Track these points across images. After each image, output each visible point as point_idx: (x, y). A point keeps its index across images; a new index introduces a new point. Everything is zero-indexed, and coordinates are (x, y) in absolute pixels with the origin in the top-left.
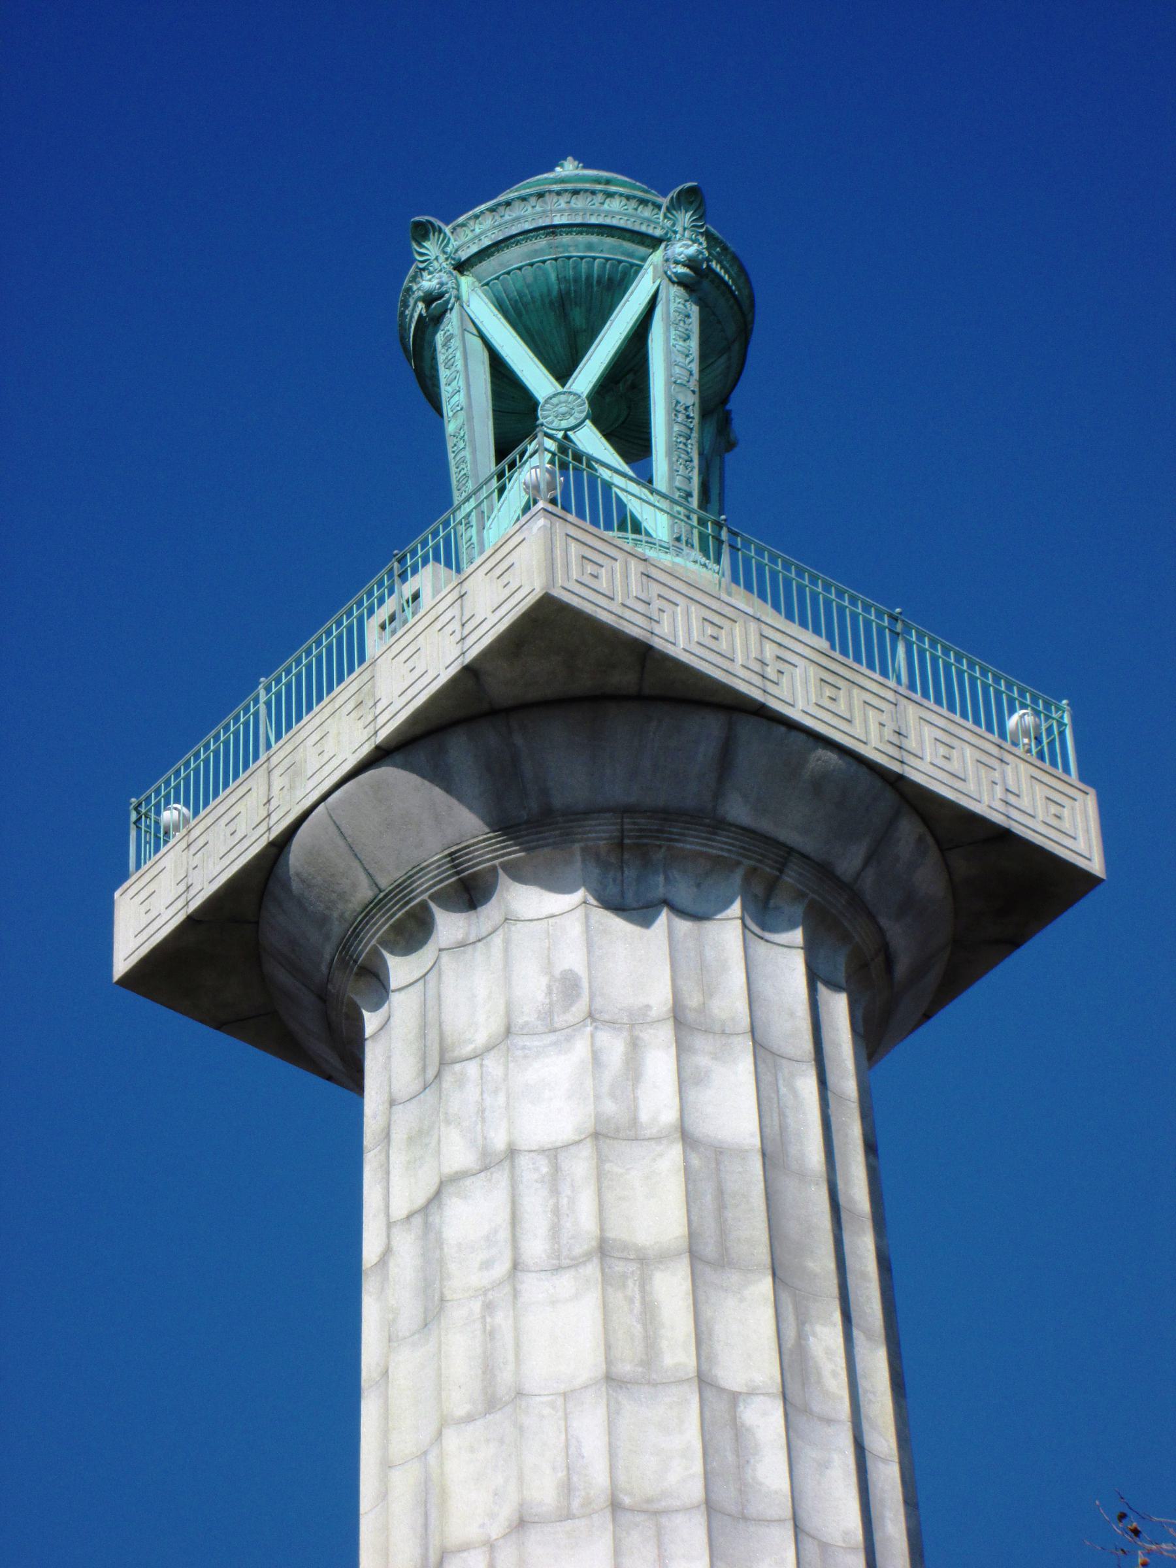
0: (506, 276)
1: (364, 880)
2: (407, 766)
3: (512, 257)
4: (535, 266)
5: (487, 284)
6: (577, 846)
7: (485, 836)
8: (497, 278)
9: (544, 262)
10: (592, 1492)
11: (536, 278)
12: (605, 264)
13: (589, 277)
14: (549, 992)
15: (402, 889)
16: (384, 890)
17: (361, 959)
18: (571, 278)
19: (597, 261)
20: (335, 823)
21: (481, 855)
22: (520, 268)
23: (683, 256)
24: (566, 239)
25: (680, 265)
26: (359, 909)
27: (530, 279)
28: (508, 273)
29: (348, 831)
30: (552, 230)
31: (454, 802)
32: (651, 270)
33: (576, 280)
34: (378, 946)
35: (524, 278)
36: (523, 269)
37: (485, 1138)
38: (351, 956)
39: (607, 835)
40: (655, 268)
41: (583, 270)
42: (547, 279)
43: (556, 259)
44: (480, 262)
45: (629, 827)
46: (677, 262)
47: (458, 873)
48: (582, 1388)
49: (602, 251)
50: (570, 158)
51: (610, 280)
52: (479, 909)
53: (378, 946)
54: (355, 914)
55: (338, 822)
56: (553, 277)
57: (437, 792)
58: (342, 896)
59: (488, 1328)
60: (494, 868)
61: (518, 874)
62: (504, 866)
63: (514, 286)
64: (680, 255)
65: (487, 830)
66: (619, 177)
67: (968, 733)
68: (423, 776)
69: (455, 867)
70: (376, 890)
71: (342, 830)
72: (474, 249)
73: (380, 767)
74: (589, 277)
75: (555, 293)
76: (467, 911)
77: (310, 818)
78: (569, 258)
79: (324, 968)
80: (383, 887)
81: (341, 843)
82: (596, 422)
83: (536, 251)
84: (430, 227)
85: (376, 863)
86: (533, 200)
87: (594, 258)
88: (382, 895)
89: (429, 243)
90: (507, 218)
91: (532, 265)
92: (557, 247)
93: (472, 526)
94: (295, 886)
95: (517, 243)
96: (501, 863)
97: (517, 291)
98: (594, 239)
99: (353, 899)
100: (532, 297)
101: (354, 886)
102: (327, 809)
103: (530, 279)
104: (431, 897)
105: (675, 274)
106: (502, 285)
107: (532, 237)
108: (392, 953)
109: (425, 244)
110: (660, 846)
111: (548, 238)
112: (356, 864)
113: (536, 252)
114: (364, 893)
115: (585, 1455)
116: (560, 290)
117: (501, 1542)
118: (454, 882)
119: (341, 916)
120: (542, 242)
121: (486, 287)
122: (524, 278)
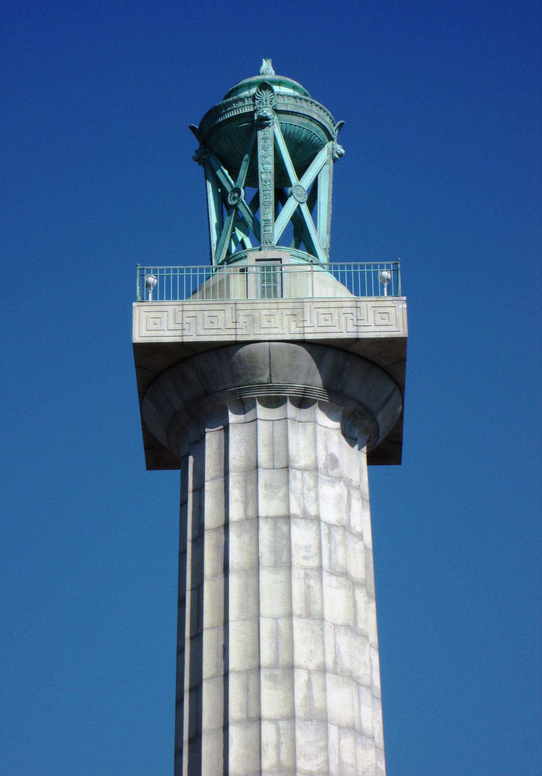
0: (290, 125)
1: (267, 376)
2: (310, 351)
3: (296, 120)
4: (300, 128)
5: (281, 123)
6: (344, 408)
7: (320, 389)
8: (286, 124)
9: (304, 129)
10: (344, 668)
11: (299, 132)
12: (318, 140)
13: (312, 141)
14: (326, 459)
15: (281, 388)
16: (273, 384)
17: (242, 397)
18: (308, 139)
19: (317, 137)
20: (270, 352)
21: (314, 394)
22: (296, 126)
23: (339, 151)
24: (314, 125)
25: (337, 154)
26: (257, 382)
27: (296, 131)
28: (291, 125)
29: (272, 357)
30: (312, 119)
31: (317, 371)
32: (327, 149)
33: (309, 140)
34: (256, 398)
35: (295, 130)
36: (296, 127)
37: (304, 506)
38: (240, 394)
39: (352, 409)
40: (328, 149)
41: (312, 138)
42: (301, 135)
43: (308, 130)
44: (283, 114)
45: (358, 409)
46: (337, 152)
47: (304, 395)
48: (340, 625)
49: (319, 135)
50: (270, 60)
51: (316, 145)
52: (302, 409)
53: (256, 398)
54: (255, 383)
55: (271, 353)
56: (303, 135)
57: (314, 365)
58: (254, 375)
59: (307, 584)
60: (316, 401)
61: (323, 407)
62: (320, 401)
63: (290, 130)
64: (339, 150)
65: (322, 387)
66: (290, 80)
67: (217, 306)
68: (313, 358)
69: (304, 392)
70: (270, 382)
71: (271, 356)
72: (284, 108)
73: (300, 346)
74: (312, 141)
75: (300, 140)
76: (297, 408)
77: (262, 343)
78: (311, 132)
79: (221, 388)
80: (273, 382)
81: (267, 360)
82: (307, 203)
83: (303, 123)
84: (269, 88)
85: (276, 374)
86: (309, 103)
87: (317, 136)
88: (271, 385)
89: (265, 92)
90: (298, 104)
91: (300, 127)
92: (310, 126)
93: (271, 226)
94: (234, 359)
95: (300, 116)
96: (320, 400)
97: (290, 132)
98: (320, 129)
99: (258, 378)
100: (293, 137)
101: (261, 375)
102: (270, 346)
103: (296, 131)
104: (290, 397)
105: (335, 156)
106: (286, 127)
107: (301, 116)
108: (259, 403)
109: (263, 91)
110: (360, 419)
111: (309, 121)
112: (268, 369)
113: (303, 124)
114: (265, 379)
115: (341, 652)
116: (302, 140)
117: (313, 672)
118: (301, 397)
119: (248, 380)
120: (306, 121)
121: (280, 124)
122: (295, 130)
